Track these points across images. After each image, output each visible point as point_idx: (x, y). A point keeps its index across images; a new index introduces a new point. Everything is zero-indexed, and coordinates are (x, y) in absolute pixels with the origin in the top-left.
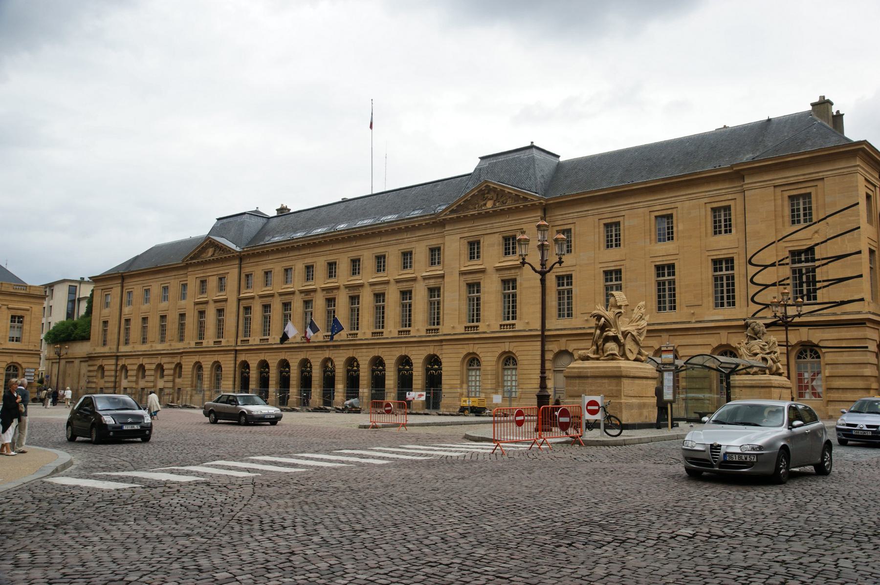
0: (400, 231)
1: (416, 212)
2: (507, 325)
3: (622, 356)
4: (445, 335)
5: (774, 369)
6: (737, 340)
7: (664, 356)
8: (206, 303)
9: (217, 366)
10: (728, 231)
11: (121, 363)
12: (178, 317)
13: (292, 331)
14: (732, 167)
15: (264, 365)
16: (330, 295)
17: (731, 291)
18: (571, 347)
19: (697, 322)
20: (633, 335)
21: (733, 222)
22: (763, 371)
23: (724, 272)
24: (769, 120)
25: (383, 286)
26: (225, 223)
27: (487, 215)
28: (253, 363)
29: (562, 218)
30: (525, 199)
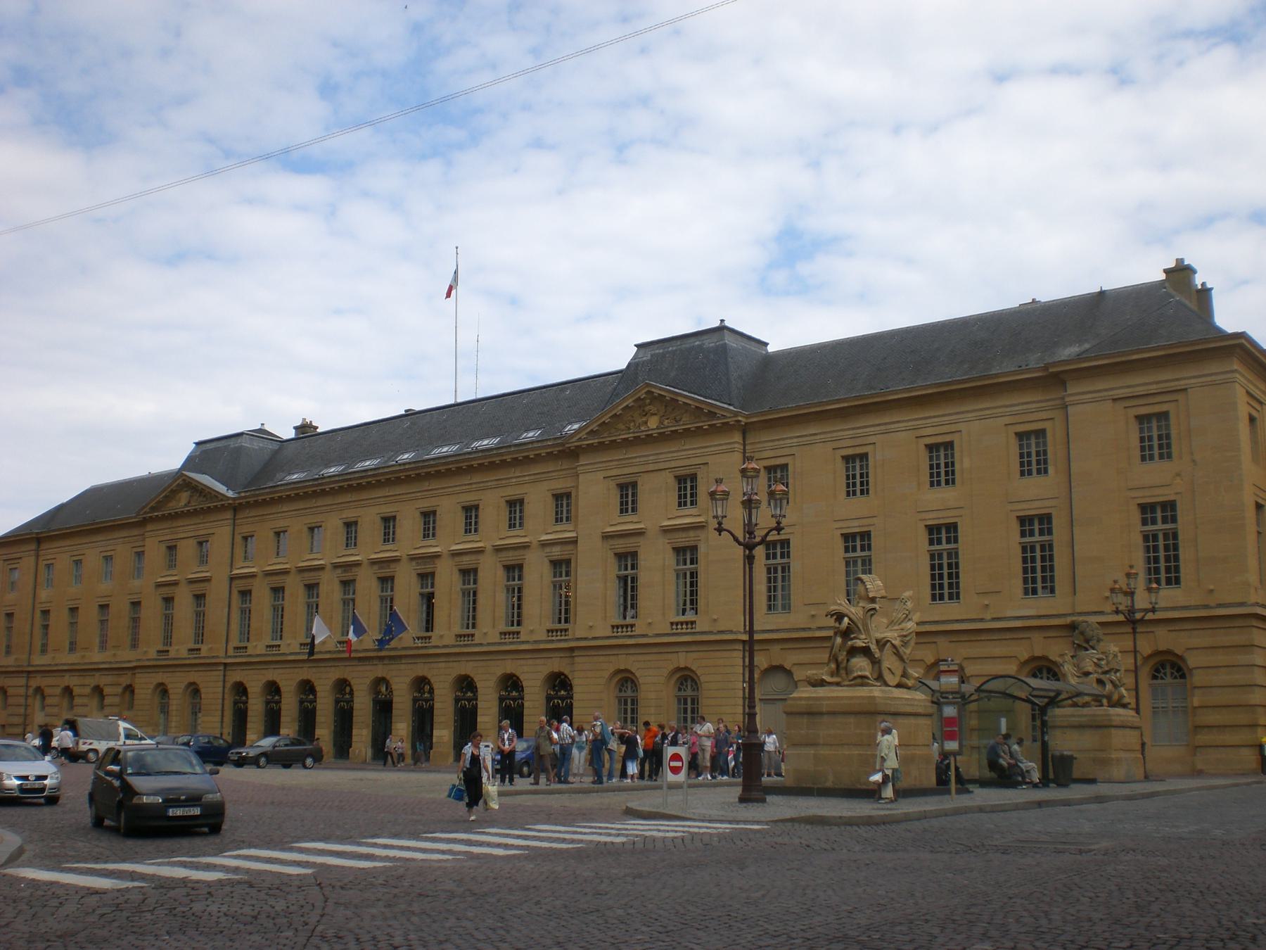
0: (504, 464)
1: (531, 434)
2: (682, 623)
3: (876, 679)
4: (578, 639)
5: (1115, 697)
6: (1057, 650)
7: (944, 679)
8: (175, 583)
9: (194, 690)
10: (1043, 471)
11: (34, 683)
12: (128, 606)
13: (321, 631)
14: (1046, 368)
15: (273, 689)
16: (385, 572)
17: (1049, 569)
18: (789, 660)
19: (994, 619)
20: (894, 646)
21: (1050, 456)
22: (1098, 699)
23: (1037, 538)
24: (1102, 293)
25: (473, 557)
26: (210, 453)
27: (650, 440)
28: (255, 684)
29: (770, 447)
30: (712, 415)
